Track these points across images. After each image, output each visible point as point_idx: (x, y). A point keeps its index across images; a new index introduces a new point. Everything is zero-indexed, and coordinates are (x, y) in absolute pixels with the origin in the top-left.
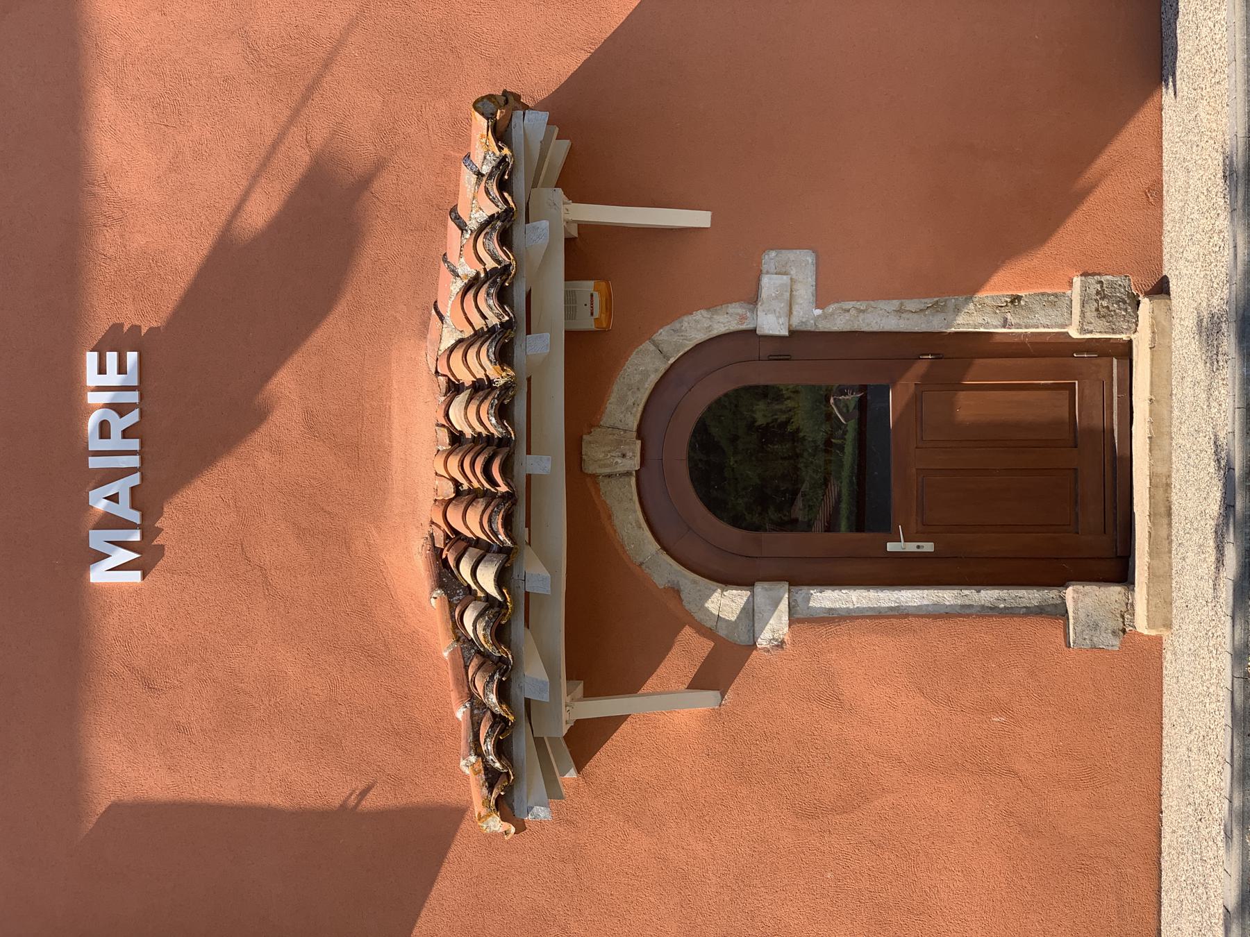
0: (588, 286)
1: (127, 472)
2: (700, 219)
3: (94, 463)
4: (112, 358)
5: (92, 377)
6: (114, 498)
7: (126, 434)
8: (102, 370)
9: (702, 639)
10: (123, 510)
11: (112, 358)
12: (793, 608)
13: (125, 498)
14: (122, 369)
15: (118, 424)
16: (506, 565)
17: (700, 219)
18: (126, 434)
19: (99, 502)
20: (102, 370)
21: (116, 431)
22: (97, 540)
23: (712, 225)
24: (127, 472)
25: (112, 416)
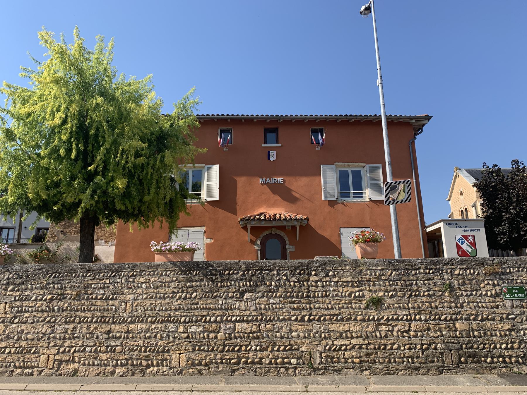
2: (298, 239)
5: (280, 179)
15: (276, 181)
17: (298, 239)
19: (268, 179)
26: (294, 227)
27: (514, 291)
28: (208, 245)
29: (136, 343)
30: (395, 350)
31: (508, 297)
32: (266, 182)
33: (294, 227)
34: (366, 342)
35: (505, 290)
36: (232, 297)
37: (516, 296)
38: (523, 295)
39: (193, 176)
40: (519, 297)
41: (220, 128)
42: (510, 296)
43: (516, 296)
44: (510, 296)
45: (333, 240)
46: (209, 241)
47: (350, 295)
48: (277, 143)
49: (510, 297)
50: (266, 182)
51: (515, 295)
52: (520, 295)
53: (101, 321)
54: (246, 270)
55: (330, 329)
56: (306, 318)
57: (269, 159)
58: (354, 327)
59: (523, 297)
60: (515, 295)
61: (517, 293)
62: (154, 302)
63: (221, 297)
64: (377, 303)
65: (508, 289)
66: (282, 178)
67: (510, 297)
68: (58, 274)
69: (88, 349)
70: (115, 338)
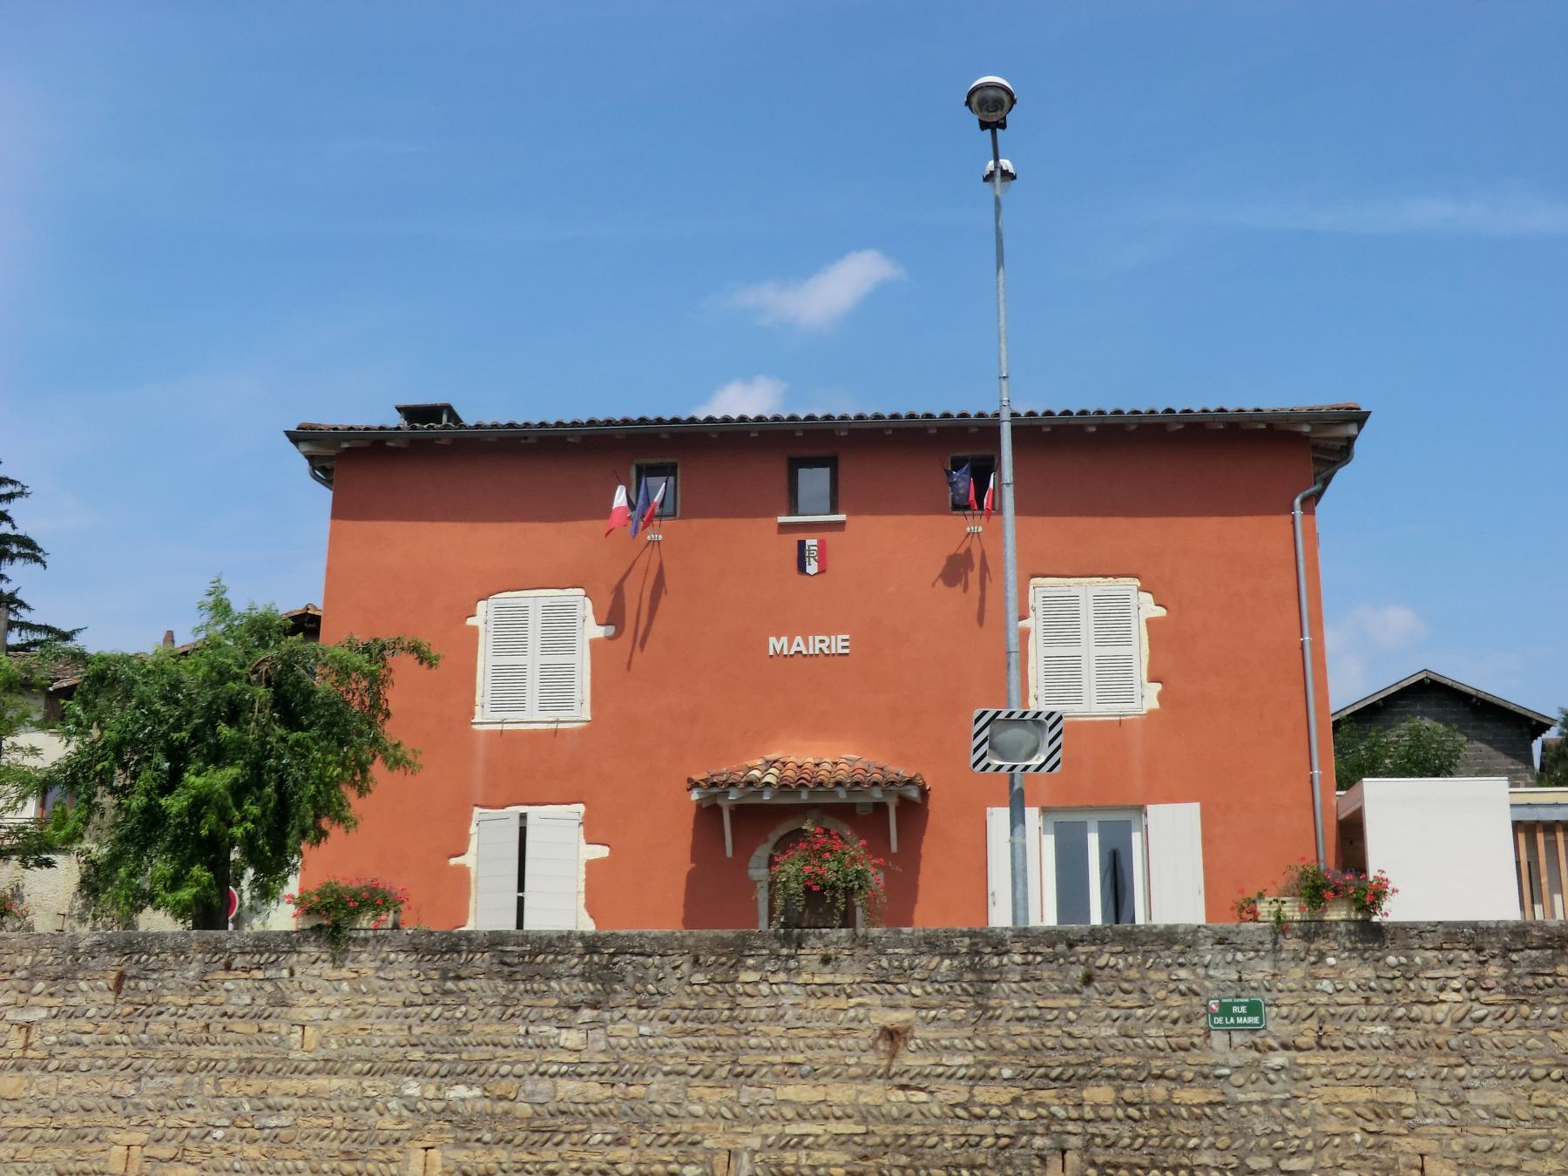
0: (871, 811)
1: (808, 649)
2: (729, 853)
3: (811, 638)
4: (847, 644)
5: (840, 637)
6: (798, 645)
7: (821, 649)
8: (843, 640)
9: (1535, 818)
10: (794, 649)
11: (847, 644)
12: (593, 1042)
13: (798, 649)
14: (843, 647)
15: (824, 646)
16: (1406, 1132)
17: (729, 853)
18: (821, 649)
19: (798, 639)
20: (843, 640)
21: (822, 645)
22: (784, 640)
23: (1188, 799)
24: (808, 649)
25: (827, 644)
26: (881, 808)
27: (1235, 1009)
28: (591, 866)
29: (326, 1122)
30: (930, 1148)
31: (1219, 1025)
32: (789, 651)
33: (881, 808)
34: (862, 1129)
35: (1214, 1006)
36: (547, 1020)
37: (1240, 1020)
38: (1256, 1020)
39: (546, 624)
40: (1245, 1025)
41: (636, 462)
42: (1224, 1020)
43: (1240, 1020)
44: (1224, 1020)
45: (1019, 518)
46: (602, 852)
47: (832, 1017)
48: (834, 510)
49: (1225, 1025)
50: (789, 651)
51: (1236, 1020)
52: (1250, 1020)
53: (249, 1068)
54: (586, 954)
55: (779, 1098)
56: (723, 1072)
57: (802, 568)
58: (840, 1094)
59: (1255, 1025)
60: (1236, 1020)
61: (1241, 1015)
62: (369, 1027)
63: (524, 1018)
64: (893, 1035)
65: (1221, 1005)
66: (847, 637)
67: (1225, 1025)
68: (145, 957)
69: (219, 1134)
70: (276, 1109)
